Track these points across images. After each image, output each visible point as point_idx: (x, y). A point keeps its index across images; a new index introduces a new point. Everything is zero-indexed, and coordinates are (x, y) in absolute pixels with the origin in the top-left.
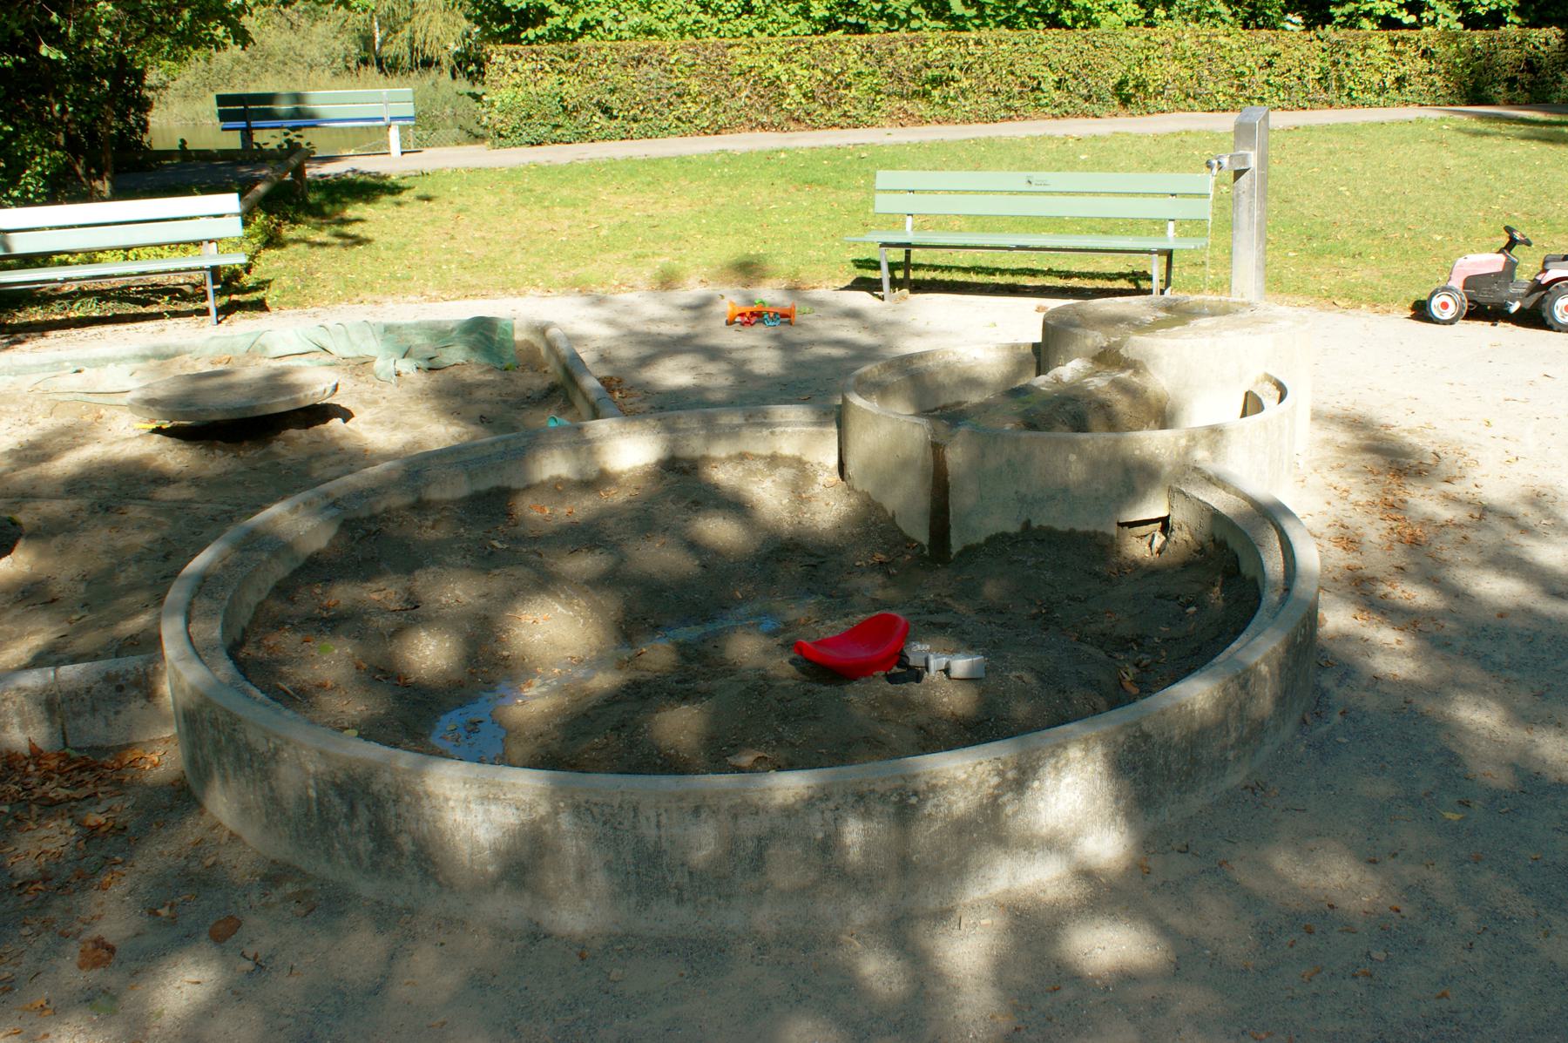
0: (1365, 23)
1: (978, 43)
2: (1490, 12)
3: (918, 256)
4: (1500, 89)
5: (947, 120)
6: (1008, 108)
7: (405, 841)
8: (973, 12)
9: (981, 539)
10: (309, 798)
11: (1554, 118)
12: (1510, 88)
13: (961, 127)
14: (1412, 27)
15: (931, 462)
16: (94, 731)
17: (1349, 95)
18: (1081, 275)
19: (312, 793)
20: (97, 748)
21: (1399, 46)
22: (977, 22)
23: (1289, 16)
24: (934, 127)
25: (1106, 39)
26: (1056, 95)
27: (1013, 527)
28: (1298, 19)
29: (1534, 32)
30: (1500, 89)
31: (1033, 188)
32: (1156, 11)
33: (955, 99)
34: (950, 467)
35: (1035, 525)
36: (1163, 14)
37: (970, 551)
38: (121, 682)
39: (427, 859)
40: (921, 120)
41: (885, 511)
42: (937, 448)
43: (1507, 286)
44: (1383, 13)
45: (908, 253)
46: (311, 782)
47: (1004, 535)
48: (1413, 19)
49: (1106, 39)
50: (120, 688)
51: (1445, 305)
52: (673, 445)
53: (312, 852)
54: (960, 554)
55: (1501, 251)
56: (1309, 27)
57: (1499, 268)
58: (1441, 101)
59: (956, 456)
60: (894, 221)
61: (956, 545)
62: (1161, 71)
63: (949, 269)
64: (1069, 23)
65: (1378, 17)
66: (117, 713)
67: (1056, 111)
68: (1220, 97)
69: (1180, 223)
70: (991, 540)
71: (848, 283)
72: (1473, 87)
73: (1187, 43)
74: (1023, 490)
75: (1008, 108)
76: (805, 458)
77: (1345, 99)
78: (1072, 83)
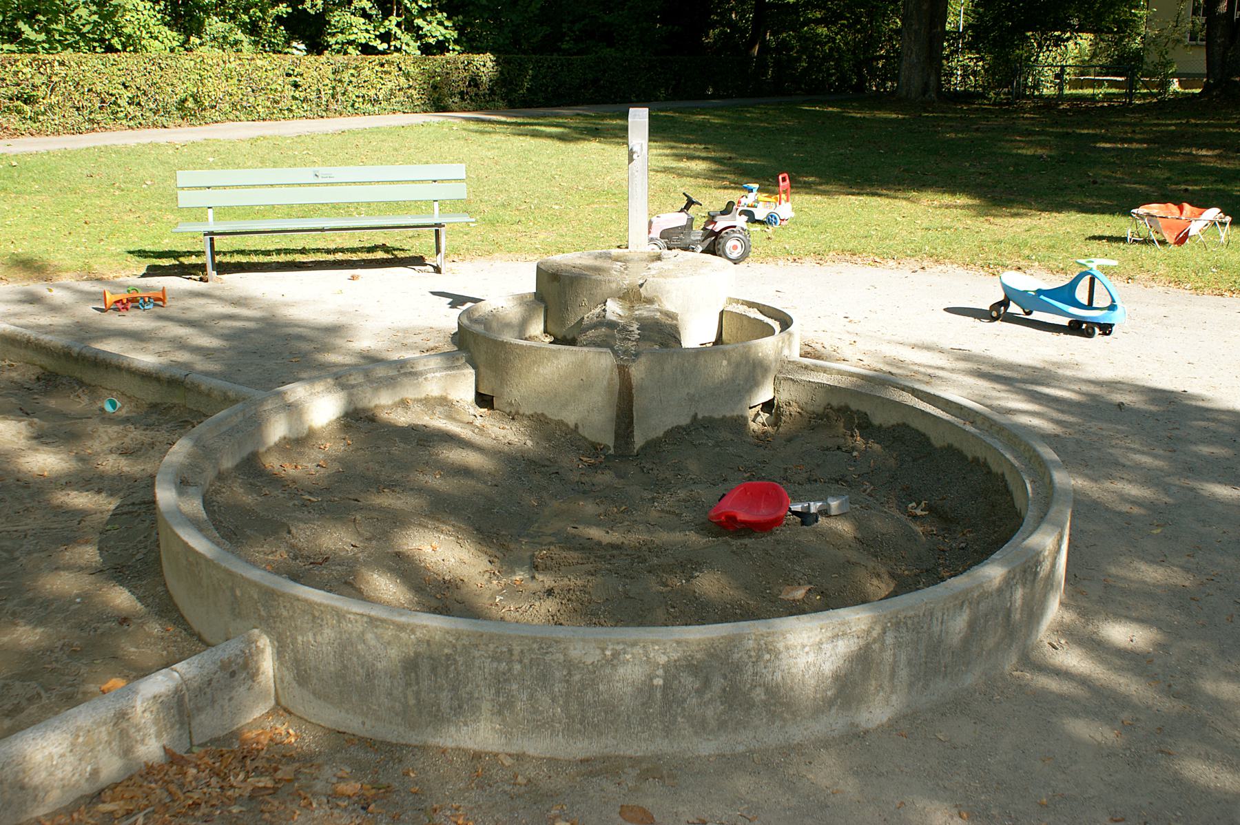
0: (351, 49)
1: (62, 64)
2: (438, 42)
3: (221, 244)
4: (456, 100)
5: (39, 132)
6: (91, 121)
7: (759, 695)
8: (43, 37)
9: (661, 434)
10: (652, 687)
11: (519, 120)
12: (463, 99)
13: (52, 138)
14: (384, 53)
15: (617, 380)
16: (208, 724)
17: (353, 106)
18: (256, 252)
19: (659, 682)
20: (218, 739)
21: (386, 67)
22: (47, 46)
23: (294, 44)
24: (28, 139)
25: (169, 62)
26: (131, 109)
27: (684, 421)
28: (302, 47)
29: (476, 57)
30: (456, 100)
31: (320, 180)
32: (192, 38)
33: (43, 114)
34: (634, 382)
35: (700, 417)
36: (198, 41)
37: (653, 446)
38: (234, 667)
39: (779, 702)
40: (16, 133)
41: (567, 425)
42: (623, 371)
43: (689, 234)
44: (363, 41)
45: (212, 239)
46: (660, 672)
47: (678, 427)
48: (385, 46)
49: (169, 62)
50: (233, 674)
51: (735, 247)
52: (350, 401)
53: (646, 735)
54: (642, 448)
55: (682, 211)
56: (309, 52)
57: (683, 222)
58: (417, 109)
59: (637, 372)
60: (197, 214)
61: (639, 440)
62: (214, 88)
63: (249, 253)
64: (119, 47)
65: (361, 44)
66: (230, 699)
67: (131, 124)
68: (260, 109)
69: (442, 203)
70: (669, 433)
71: (144, 271)
72: (437, 99)
73: (233, 65)
74: (692, 391)
75: (91, 121)
76: (450, 397)
77: (350, 109)
78: (143, 100)
